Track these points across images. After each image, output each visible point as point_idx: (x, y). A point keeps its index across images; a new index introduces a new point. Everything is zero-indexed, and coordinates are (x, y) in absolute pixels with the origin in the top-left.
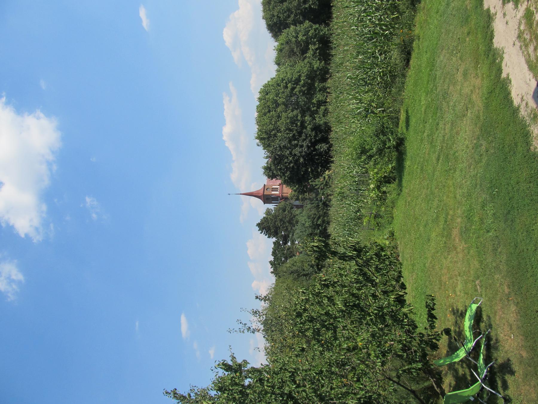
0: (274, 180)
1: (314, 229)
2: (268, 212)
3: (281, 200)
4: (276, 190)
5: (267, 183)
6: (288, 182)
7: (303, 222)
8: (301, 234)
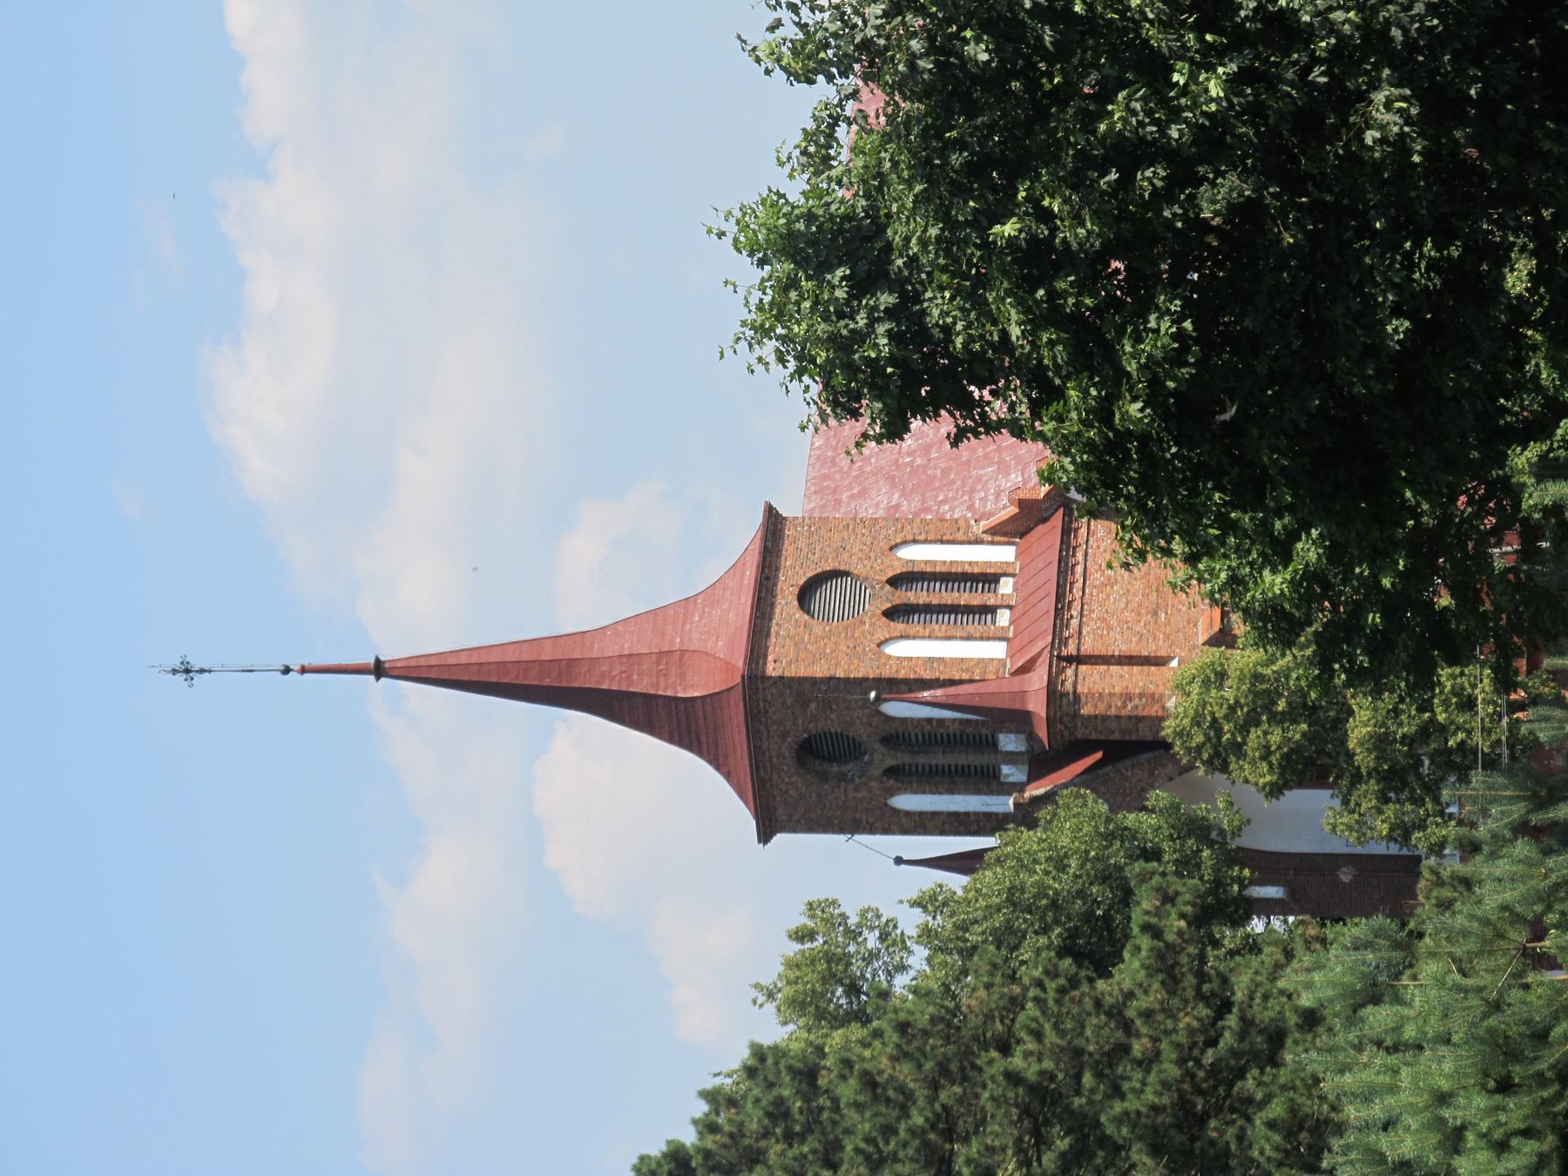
3: (1040, 763)
4: (953, 598)
5: (819, 487)
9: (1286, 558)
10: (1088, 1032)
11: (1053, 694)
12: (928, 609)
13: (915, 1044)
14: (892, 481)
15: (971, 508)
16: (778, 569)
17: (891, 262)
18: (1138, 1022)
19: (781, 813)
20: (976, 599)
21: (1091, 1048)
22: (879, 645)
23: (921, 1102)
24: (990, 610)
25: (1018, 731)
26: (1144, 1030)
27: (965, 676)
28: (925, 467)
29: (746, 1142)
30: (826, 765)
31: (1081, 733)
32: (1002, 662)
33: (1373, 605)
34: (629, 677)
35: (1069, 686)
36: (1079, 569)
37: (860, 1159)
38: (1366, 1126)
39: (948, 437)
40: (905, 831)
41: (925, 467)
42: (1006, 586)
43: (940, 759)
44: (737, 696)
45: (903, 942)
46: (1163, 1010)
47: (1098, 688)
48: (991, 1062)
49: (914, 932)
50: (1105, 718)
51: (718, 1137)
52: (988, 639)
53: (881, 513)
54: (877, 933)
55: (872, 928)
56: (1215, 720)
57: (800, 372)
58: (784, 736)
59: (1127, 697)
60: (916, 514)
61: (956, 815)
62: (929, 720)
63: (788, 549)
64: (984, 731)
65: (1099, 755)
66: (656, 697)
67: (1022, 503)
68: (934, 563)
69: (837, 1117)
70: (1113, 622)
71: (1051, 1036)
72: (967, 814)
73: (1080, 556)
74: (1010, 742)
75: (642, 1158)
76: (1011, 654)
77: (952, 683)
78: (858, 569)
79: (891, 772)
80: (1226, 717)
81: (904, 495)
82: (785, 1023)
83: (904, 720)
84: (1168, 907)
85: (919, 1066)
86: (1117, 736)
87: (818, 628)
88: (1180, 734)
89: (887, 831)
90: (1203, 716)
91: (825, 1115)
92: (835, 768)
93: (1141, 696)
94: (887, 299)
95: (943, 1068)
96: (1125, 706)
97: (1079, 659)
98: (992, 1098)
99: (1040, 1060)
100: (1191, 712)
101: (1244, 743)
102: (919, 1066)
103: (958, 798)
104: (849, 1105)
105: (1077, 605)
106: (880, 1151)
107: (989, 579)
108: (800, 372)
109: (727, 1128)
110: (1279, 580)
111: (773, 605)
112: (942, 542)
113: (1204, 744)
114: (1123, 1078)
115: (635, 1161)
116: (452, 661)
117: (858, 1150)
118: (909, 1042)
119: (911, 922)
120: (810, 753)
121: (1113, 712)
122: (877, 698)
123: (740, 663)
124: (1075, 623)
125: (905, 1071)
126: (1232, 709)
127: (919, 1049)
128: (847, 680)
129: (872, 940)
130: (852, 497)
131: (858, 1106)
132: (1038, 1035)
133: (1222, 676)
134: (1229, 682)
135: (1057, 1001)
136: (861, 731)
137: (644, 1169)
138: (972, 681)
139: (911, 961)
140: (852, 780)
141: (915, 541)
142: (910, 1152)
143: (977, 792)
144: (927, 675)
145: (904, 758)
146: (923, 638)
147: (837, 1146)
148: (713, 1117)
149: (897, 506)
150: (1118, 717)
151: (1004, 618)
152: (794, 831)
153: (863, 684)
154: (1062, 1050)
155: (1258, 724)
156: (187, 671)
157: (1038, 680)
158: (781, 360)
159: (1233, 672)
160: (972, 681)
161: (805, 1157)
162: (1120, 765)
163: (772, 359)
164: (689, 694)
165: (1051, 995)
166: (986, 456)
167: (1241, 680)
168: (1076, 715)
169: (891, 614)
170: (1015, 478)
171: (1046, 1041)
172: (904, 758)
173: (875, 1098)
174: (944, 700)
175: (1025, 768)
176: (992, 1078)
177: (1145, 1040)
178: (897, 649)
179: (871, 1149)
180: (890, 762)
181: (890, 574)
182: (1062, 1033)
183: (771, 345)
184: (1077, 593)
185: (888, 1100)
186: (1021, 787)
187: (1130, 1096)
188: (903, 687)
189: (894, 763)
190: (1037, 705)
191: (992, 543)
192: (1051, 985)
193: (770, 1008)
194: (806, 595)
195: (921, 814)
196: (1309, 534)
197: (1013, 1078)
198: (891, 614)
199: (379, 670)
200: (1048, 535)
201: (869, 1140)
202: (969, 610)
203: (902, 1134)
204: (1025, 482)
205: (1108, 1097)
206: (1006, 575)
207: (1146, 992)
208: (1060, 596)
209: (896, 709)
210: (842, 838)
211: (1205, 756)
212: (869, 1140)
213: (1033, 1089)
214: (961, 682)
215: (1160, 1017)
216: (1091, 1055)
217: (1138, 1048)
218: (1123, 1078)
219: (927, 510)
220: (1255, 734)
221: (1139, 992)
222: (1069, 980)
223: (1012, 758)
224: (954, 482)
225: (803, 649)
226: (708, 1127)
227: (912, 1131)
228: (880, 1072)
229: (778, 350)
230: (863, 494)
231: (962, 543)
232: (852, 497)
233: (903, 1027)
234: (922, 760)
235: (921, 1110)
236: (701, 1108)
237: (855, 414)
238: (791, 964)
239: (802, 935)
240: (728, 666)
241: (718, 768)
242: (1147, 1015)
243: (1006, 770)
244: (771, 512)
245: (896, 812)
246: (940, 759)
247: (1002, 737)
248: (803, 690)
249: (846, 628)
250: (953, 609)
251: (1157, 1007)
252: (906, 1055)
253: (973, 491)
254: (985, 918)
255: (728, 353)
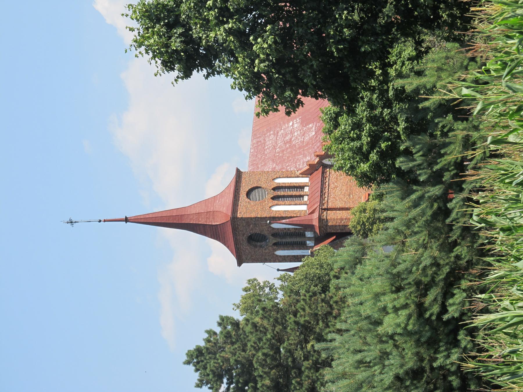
0: (198, 75)
1: (432, 344)
2: (255, 297)
3: (318, 240)
4: (292, 193)
5: (252, 163)
6: (278, 85)
7: (367, 310)
8: (361, 375)
9: (368, 160)
10: (319, 309)
11: (320, 219)
12: (284, 197)
13: (268, 314)
14: (273, 161)
15: (296, 167)
16: (240, 187)
17: (181, 17)
18: (334, 305)
19: (244, 257)
20: (298, 193)
21: (320, 313)
22: (270, 207)
23: (270, 331)
24: (302, 196)
25: (311, 231)
26: (336, 307)
27: (295, 215)
28: (283, 156)
29: (219, 345)
30: (256, 243)
31: (329, 231)
32: (306, 211)
33: (394, 172)
34: (199, 219)
35: (325, 217)
36: (327, 183)
37: (252, 349)
38: (355, 305)
39: (204, 75)
40: (280, 262)
41: (283, 156)
42: (306, 189)
43: (289, 240)
44: (229, 223)
45: (276, 290)
46: (341, 301)
47: (333, 217)
48: (290, 318)
49: (279, 287)
50: (336, 226)
51: (210, 344)
52: (302, 204)
53: (270, 170)
54: (269, 288)
55: (267, 287)
56: (363, 222)
57: (154, 57)
58: (243, 235)
59: (342, 219)
60: (280, 170)
61: (294, 256)
62: (285, 229)
63: (243, 181)
64: (301, 231)
65: (334, 237)
66: (206, 225)
67: (310, 165)
68: (285, 183)
69: (245, 337)
70: (337, 198)
71: (308, 310)
72: (297, 256)
73: (327, 179)
74: (309, 234)
75: (189, 351)
76: (308, 209)
77: (291, 217)
78: (263, 186)
79: (275, 244)
80: (367, 221)
81: (277, 164)
82: (242, 315)
83: (278, 229)
84: (342, 270)
85: (269, 320)
86: (339, 231)
87: (252, 203)
88: (353, 227)
89: (275, 261)
90: (360, 221)
91: (242, 336)
92: (259, 244)
93: (346, 219)
94: (180, 30)
95: (276, 320)
96: (341, 222)
97: (327, 209)
98: (291, 329)
99: (305, 317)
100: (356, 221)
101: (372, 229)
102: (269, 320)
103: (294, 251)
104: (248, 333)
105: (327, 194)
106: (258, 346)
107: (301, 187)
108: (154, 57)
109: (213, 341)
110: (366, 166)
111: (239, 197)
112: (287, 177)
113: (360, 230)
114: (329, 321)
115: (187, 352)
116: (147, 217)
117: (252, 346)
118: (266, 313)
119: (278, 284)
120: (251, 239)
121: (338, 224)
122: (270, 223)
123: (230, 214)
124: (326, 199)
125: (265, 322)
126: (368, 219)
127: (268, 315)
128: (261, 218)
129: (267, 290)
130: (262, 166)
131: (251, 333)
132: (304, 310)
133: (365, 210)
134: (367, 211)
135: (310, 300)
136: (266, 233)
137: (189, 354)
138: (297, 217)
139: (278, 296)
140: (264, 247)
141: (280, 177)
142: (267, 346)
143: (300, 249)
144: (284, 216)
145: (279, 240)
146: (283, 205)
147: (246, 345)
148: (209, 338)
149: (275, 168)
150: (339, 226)
151: (306, 198)
152: (248, 262)
153: (265, 219)
154: (312, 314)
155: (376, 223)
156: (71, 222)
157: (316, 215)
158: (147, 53)
159: (368, 209)
160: (297, 217)
161: (236, 348)
162: (340, 240)
163: (144, 52)
164: (216, 224)
165: (308, 298)
166: (300, 152)
167: (370, 211)
168: (327, 225)
169: (273, 198)
170: (308, 158)
171: (307, 312)
172: (279, 240)
173: (257, 331)
174: (289, 222)
175: (314, 242)
176: (290, 323)
177: (336, 310)
178: (275, 208)
179: (256, 345)
180: (275, 241)
181: (273, 187)
182: (311, 309)
183: (143, 48)
184: (327, 190)
185: (261, 331)
186: (312, 247)
187: (331, 327)
188: (277, 219)
189: (276, 241)
190: (316, 223)
191: (302, 177)
192: (308, 295)
193: (238, 310)
194: (248, 194)
195: (284, 256)
196: (373, 152)
197: (297, 323)
198: (273, 198)
199: (126, 220)
200: (318, 174)
201: (255, 343)
202: (296, 196)
203: (264, 341)
204: (311, 159)
205: (326, 327)
206: (306, 186)
207: (336, 296)
208: (321, 192)
209: (275, 226)
210: (262, 264)
211: (361, 233)
212: (255, 343)
213: (303, 326)
214: (294, 217)
215: (340, 303)
216: (320, 315)
217: (335, 312)
218: (329, 321)
219: (283, 168)
220: (375, 226)
221: (334, 296)
222: (313, 293)
223: (310, 239)
224: (291, 160)
225: (248, 209)
226: (208, 341)
227: (267, 340)
228: (258, 323)
229: (146, 49)
230: (265, 164)
231: (293, 177)
232: (262, 166)
233: (264, 309)
234: (284, 240)
235: (270, 333)
236: (206, 336)
237: (173, 69)
238: (244, 298)
239: (246, 290)
240: (226, 215)
241: (225, 245)
242: (336, 302)
243: (308, 242)
244: (238, 171)
245: (277, 256)
246: (289, 240)
247: (306, 233)
248: (248, 221)
249: (260, 203)
250: (291, 196)
251: (339, 300)
252: (265, 317)
253: (296, 162)
254: (299, 283)
255: (128, 51)
